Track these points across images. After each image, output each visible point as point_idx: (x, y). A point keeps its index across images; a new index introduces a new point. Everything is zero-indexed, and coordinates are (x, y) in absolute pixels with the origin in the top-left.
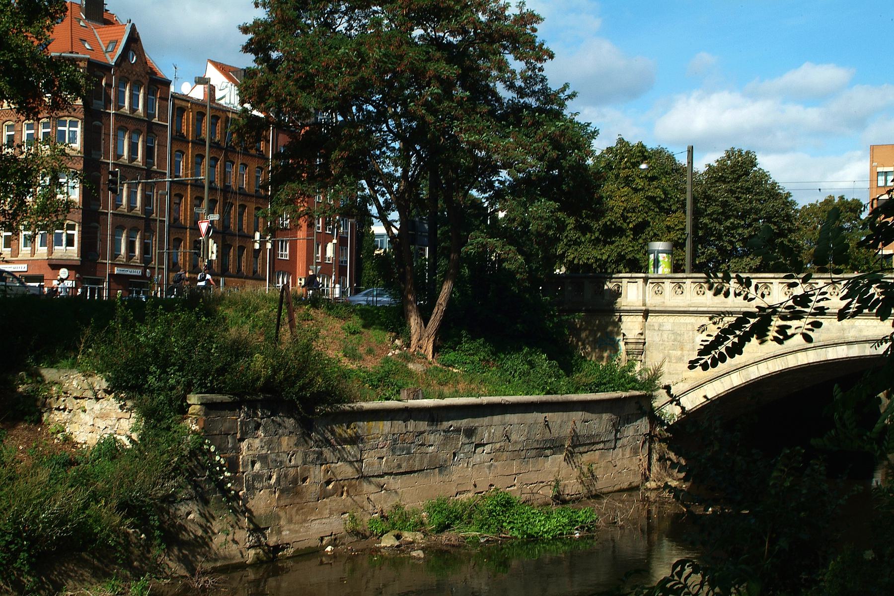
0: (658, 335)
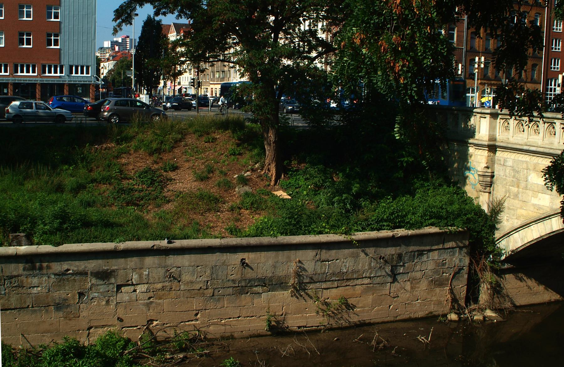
0: (503, 170)
